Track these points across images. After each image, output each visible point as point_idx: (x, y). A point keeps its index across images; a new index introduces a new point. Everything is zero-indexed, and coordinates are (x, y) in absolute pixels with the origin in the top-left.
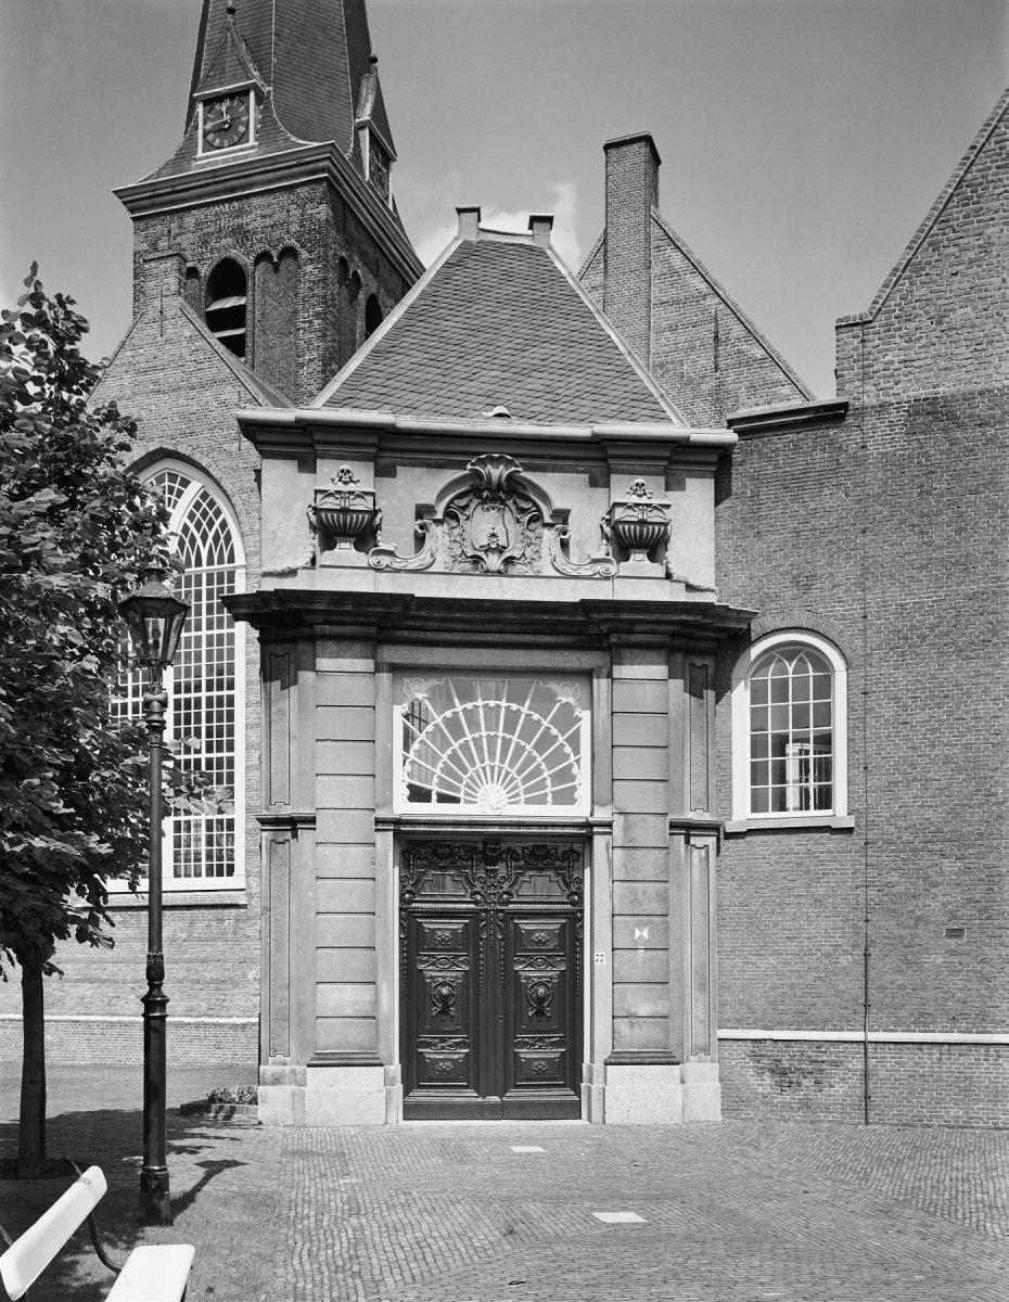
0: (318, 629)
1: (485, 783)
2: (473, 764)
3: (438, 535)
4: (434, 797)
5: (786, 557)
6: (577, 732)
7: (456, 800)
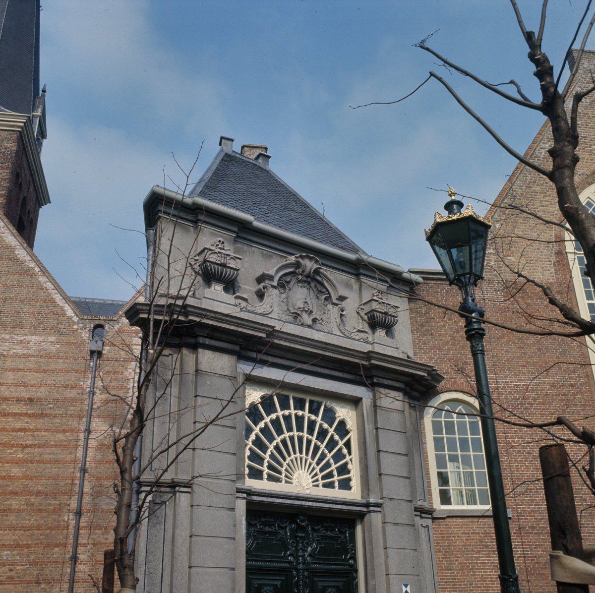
0: (201, 340)
1: (297, 469)
2: (295, 453)
3: (273, 296)
4: (265, 476)
5: (449, 349)
6: (349, 441)
7: (278, 480)
